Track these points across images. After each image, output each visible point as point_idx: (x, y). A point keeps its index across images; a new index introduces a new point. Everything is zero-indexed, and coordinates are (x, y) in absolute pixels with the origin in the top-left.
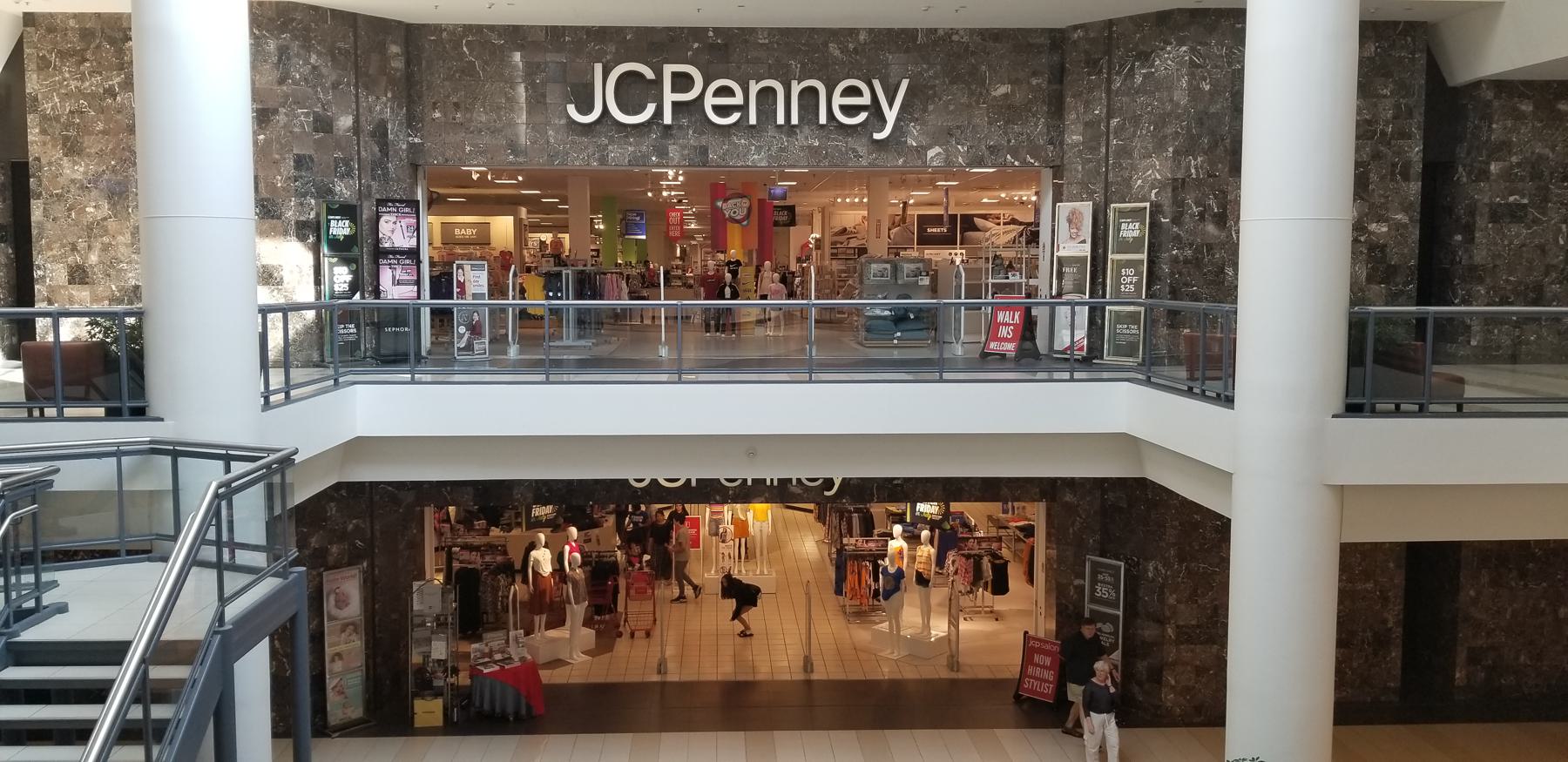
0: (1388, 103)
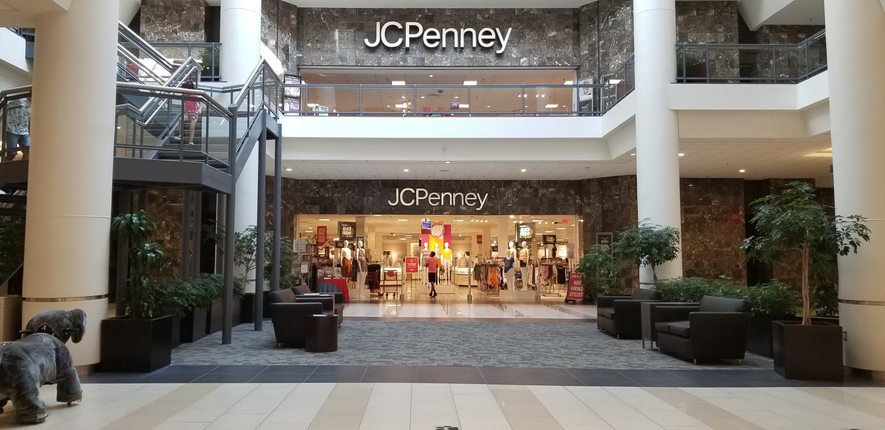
0: (722, 35)
